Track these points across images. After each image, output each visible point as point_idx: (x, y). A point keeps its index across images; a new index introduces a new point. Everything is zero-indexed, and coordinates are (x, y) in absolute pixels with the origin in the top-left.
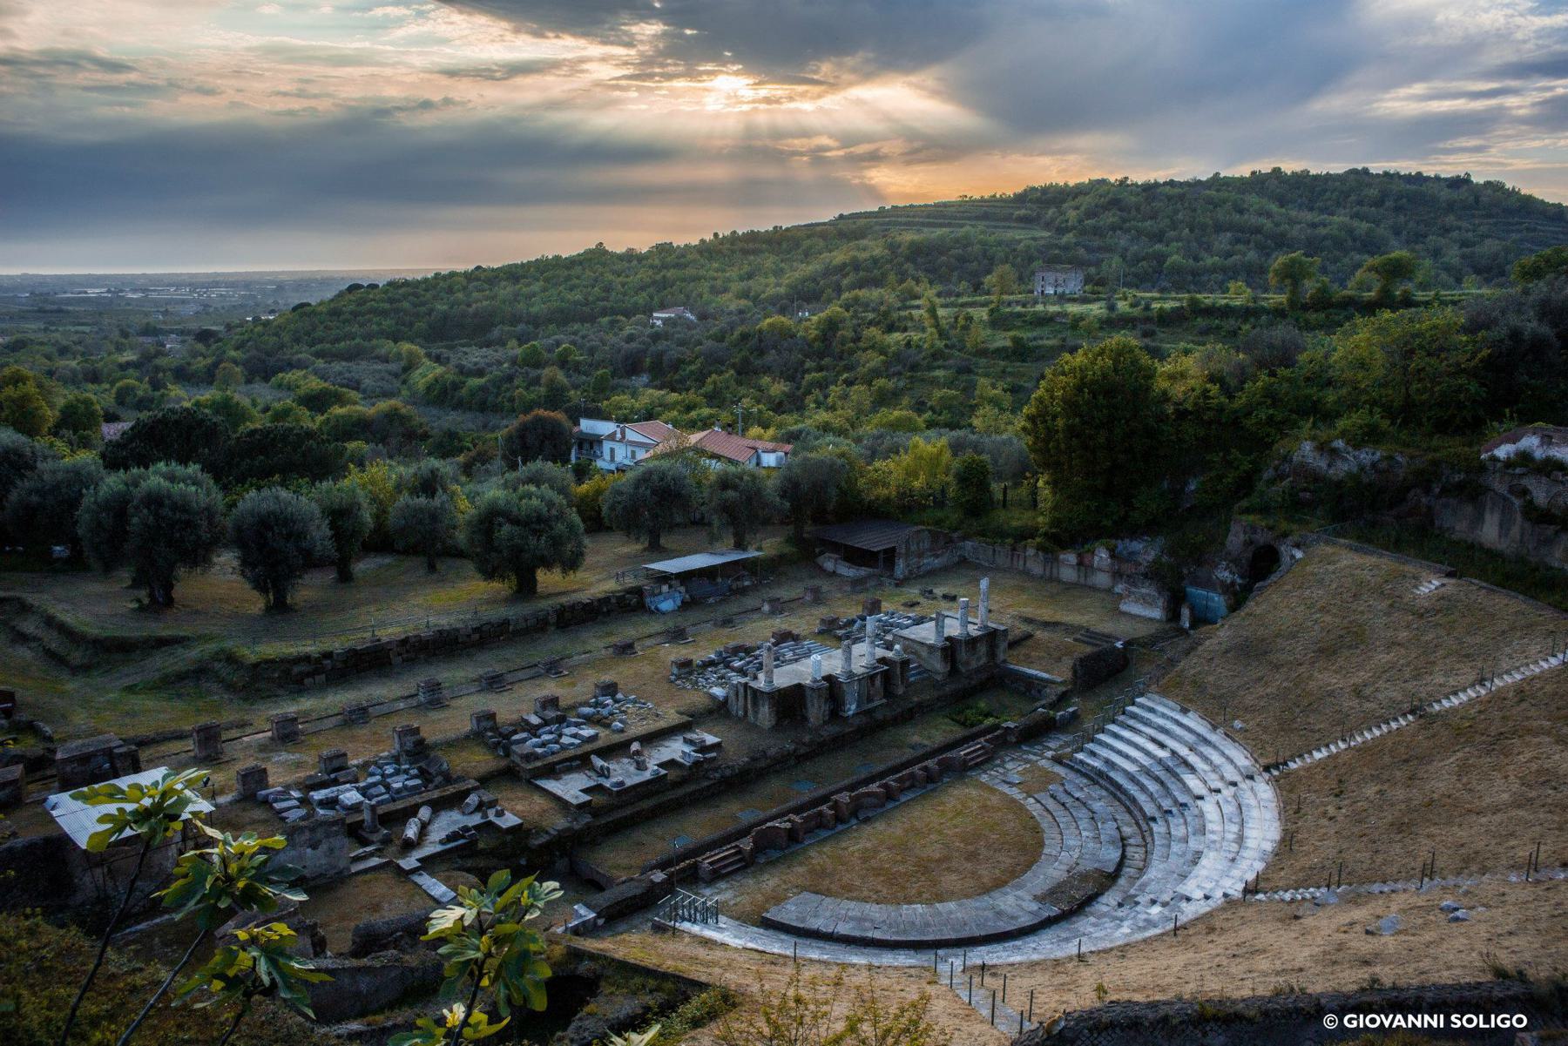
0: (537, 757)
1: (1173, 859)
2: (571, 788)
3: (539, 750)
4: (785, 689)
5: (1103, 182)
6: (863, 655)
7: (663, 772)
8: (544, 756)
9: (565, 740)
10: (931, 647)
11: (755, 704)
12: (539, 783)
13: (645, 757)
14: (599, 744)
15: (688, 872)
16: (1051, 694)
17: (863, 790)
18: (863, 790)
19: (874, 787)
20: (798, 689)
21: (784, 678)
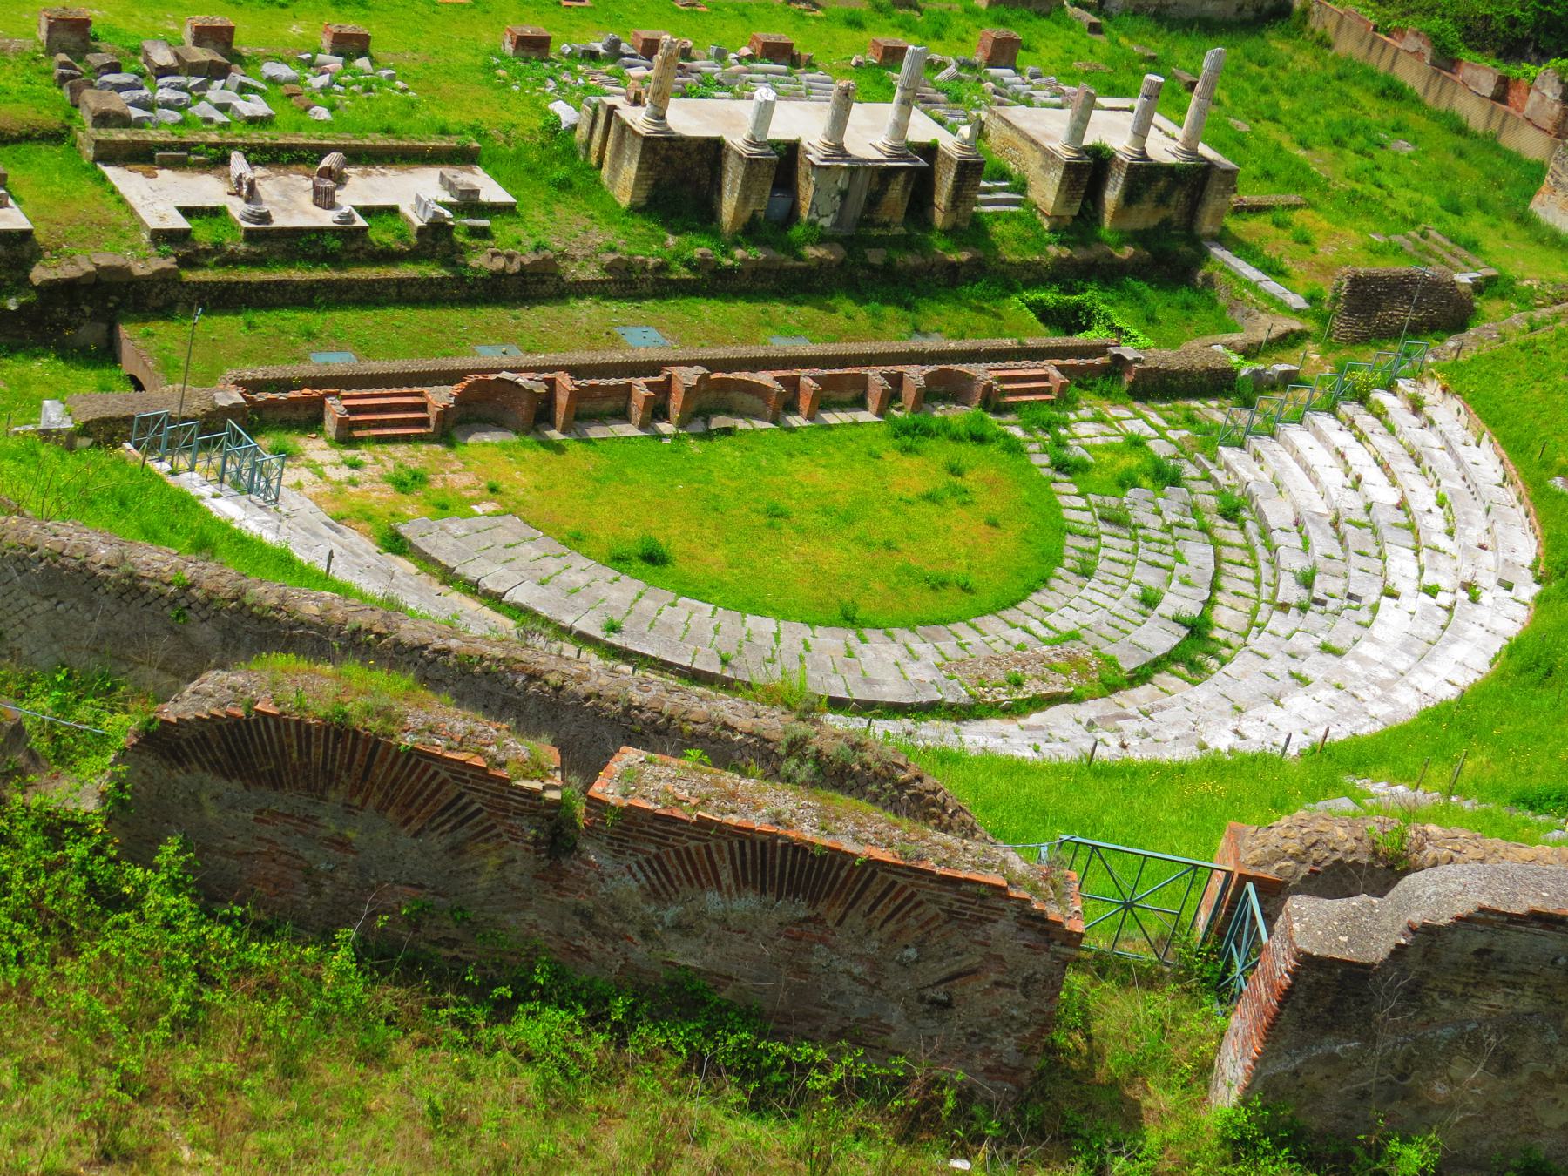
0: (124, 121)
1: (1490, 848)
2: (157, 198)
3: (136, 113)
4: (682, 139)
5: (124, 271)
6: (871, 134)
7: (360, 222)
8: (139, 124)
9: (202, 109)
10: (1049, 155)
11: (618, 152)
12: (110, 172)
13: (340, 180)
14: (265, 137)
15: (280, 411)
16: (1265, 327)
17: (745, 376)
18: (745, 376)
19: (765, 378)
20: (713, 149)
21: (689, 119)
